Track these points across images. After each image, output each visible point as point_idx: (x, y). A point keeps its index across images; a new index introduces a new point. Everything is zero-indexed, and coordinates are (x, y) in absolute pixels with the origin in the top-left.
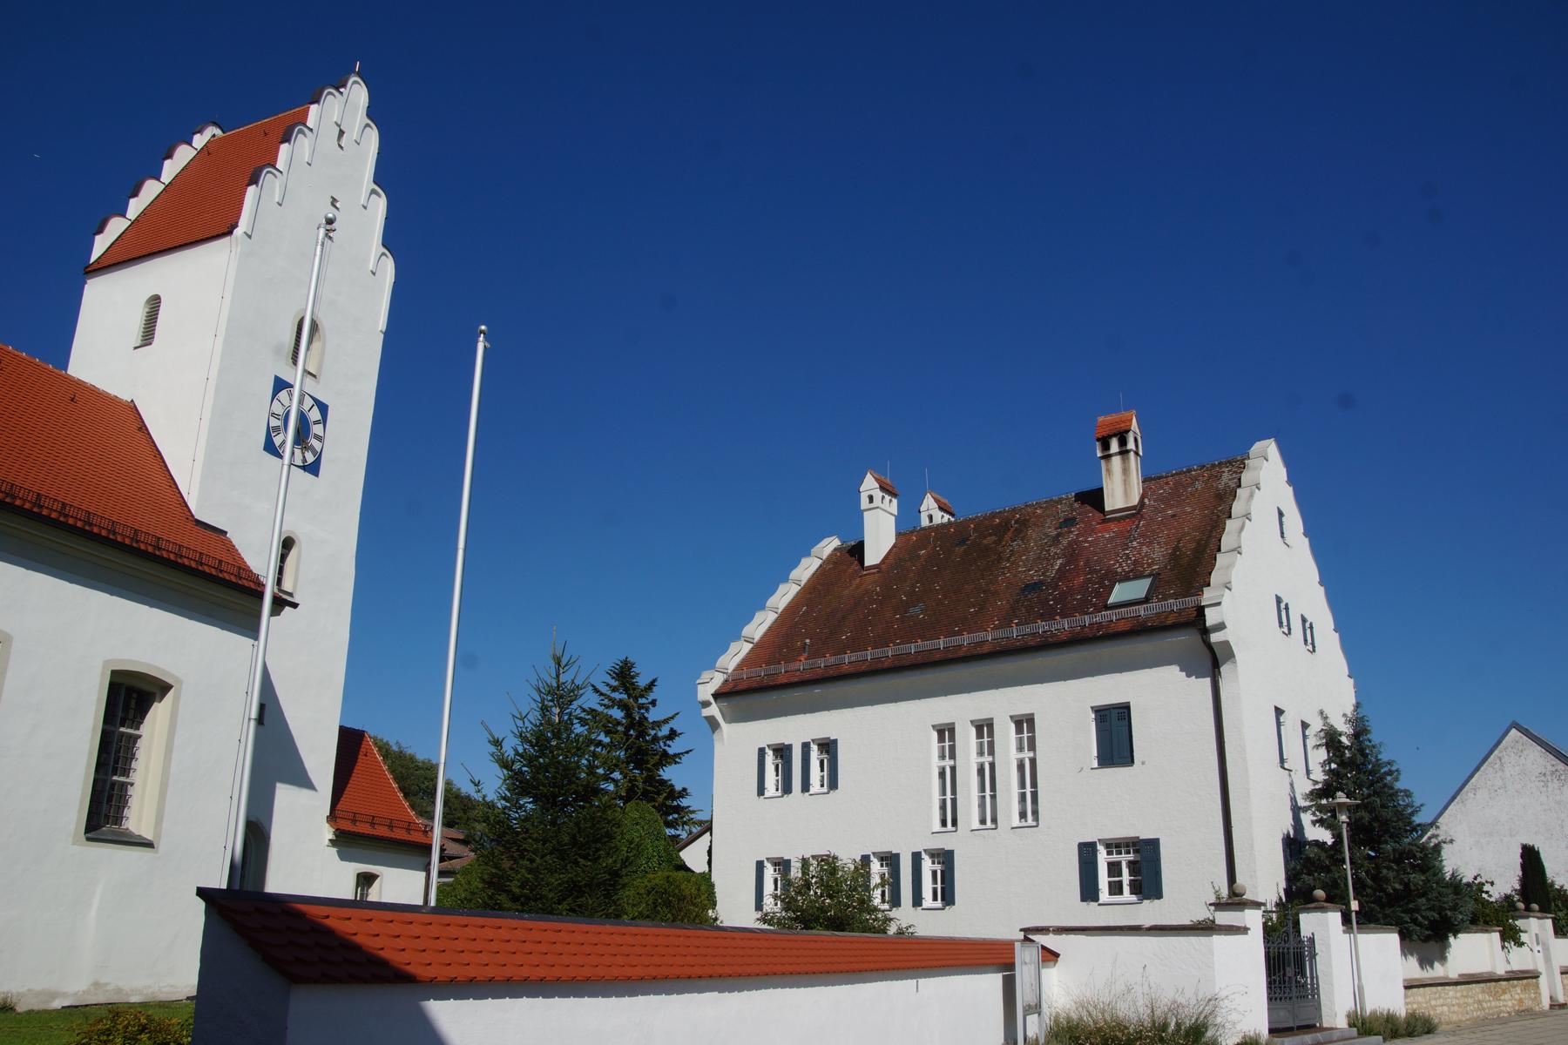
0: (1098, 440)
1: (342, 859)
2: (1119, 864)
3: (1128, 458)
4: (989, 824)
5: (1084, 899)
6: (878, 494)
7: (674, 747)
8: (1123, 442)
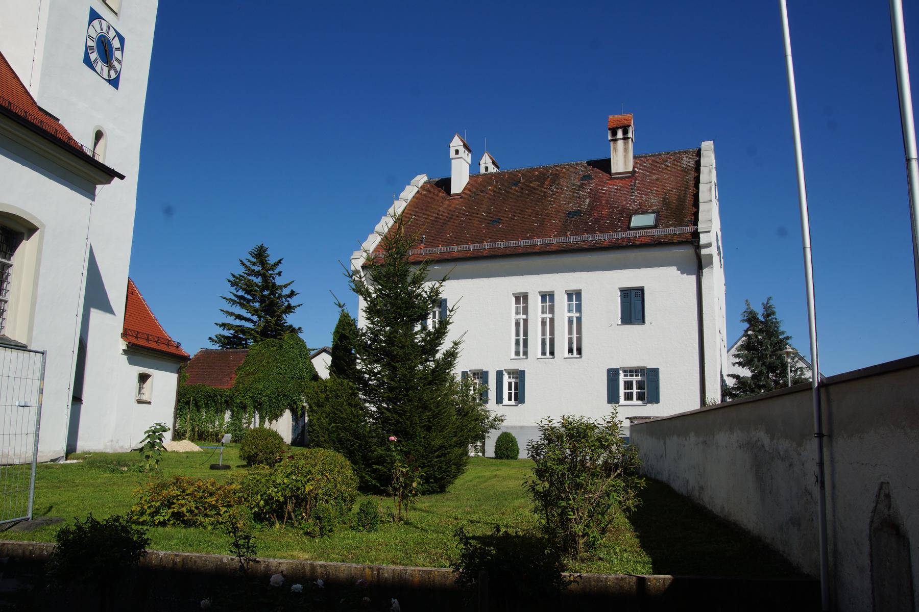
0: (610, 129)
1: (130, 364)
2: (631, 382)
3: (628, 143)
4: (548, 355)
5: (609, 402)
6: (462, 149)
7: (293, 302)
8: (625, 132)
